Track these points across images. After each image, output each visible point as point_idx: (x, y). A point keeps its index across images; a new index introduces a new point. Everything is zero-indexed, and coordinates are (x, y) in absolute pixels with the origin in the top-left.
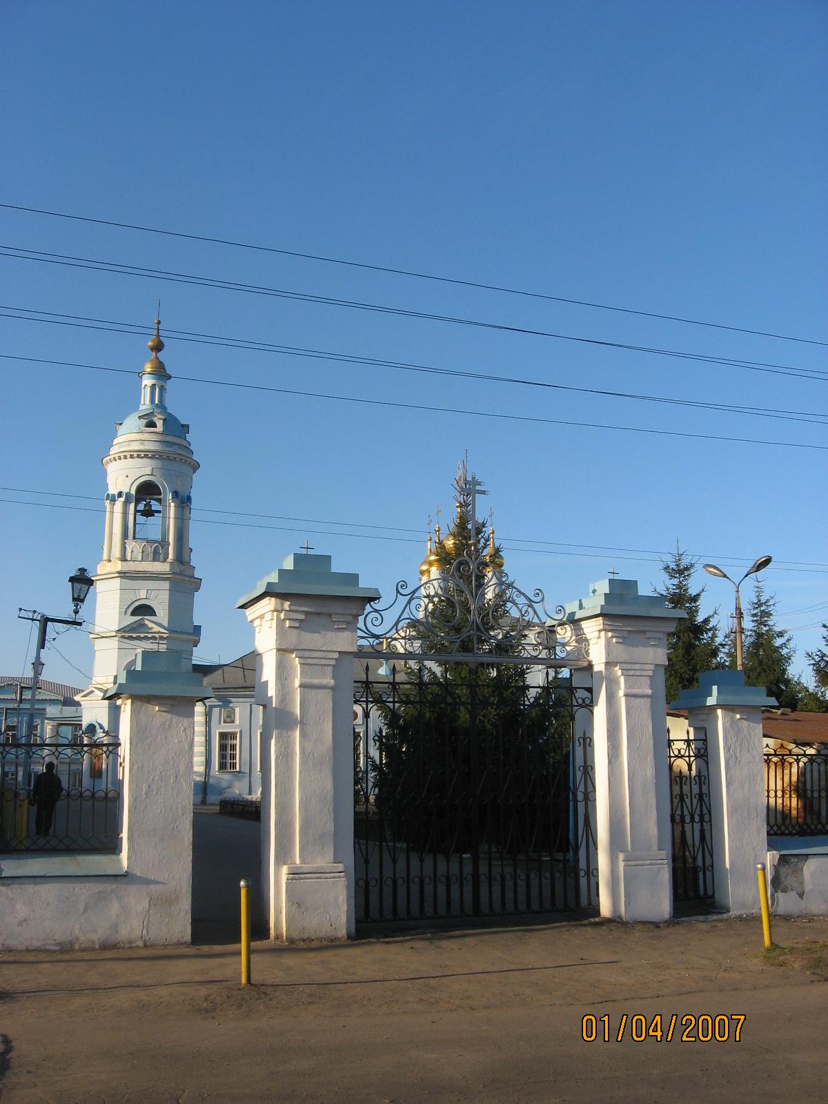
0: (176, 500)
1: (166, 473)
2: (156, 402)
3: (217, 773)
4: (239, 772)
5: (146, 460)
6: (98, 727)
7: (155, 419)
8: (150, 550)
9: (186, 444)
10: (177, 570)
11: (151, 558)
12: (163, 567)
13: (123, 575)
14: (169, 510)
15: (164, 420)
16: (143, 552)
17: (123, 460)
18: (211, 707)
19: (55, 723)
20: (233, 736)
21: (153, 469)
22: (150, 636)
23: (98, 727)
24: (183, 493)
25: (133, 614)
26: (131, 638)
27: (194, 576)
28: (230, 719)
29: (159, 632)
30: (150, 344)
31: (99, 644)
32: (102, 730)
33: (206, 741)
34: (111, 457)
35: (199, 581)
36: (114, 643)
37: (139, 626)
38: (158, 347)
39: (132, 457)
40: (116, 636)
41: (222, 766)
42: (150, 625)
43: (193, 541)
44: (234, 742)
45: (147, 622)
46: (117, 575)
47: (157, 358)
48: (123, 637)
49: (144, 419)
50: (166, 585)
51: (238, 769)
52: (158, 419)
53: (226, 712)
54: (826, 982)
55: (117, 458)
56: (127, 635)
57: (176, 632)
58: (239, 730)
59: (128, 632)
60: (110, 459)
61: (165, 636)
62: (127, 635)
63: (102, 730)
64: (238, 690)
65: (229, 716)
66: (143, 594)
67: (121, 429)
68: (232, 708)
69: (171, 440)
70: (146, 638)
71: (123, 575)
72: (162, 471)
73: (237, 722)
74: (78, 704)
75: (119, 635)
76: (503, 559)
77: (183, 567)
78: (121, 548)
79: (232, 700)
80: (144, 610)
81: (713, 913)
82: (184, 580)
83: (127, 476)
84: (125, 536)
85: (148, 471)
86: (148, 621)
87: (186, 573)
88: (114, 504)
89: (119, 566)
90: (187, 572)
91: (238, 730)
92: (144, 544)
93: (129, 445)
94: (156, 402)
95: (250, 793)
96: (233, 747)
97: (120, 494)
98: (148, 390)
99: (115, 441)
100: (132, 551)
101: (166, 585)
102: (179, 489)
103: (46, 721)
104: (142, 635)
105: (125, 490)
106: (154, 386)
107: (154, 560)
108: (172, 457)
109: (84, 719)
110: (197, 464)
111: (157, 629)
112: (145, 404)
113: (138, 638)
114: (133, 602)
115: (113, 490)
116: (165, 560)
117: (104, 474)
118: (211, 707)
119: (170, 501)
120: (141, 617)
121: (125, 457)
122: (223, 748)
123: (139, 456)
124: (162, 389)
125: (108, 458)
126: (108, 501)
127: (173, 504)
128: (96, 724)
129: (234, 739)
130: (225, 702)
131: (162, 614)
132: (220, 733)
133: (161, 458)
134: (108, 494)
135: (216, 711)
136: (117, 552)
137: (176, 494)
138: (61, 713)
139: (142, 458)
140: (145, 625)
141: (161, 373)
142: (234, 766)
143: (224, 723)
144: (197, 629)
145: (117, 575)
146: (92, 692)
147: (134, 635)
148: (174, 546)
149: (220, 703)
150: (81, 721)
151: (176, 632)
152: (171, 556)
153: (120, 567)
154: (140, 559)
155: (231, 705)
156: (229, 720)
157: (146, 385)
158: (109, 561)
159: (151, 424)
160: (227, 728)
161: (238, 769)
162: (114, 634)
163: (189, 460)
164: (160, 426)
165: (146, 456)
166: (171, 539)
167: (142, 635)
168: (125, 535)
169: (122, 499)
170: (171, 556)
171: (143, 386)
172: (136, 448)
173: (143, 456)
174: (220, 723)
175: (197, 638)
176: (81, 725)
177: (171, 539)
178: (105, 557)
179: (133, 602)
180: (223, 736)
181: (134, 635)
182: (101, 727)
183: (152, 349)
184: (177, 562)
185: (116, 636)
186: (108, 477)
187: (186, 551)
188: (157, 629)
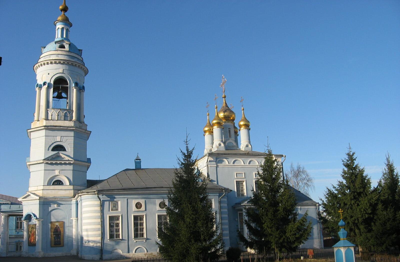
0: (77, 87)
1: (71, 73)
2: (65, 37)
3: (108, 241)
4: (122, 240)
5: (59, 65)
6: (33, 216)
7: (64, 44)
8: (62, 114)
9: (81, 59)
10: (78, 126)
11: (63, 118)
12: (71, 124)
13: (47, 128)
14: (73, 92)
15: (70, 45)
16: (58, 115)
17: (46, 65)
18: (104, 201)
19: (7, 214)
20: (117, 218)
21: (63, 70)
22: (63, 162)
23: (33, 216)
24: (81, 84)
25: (53, 150)
26: (52, 164)
27: (87, 130)
28: (115, 208)
29: (69, 160)
30: (61, 7)
31: (32, 168)
32: (35, 218)
33: (101, 221)
34: (39, 64)
35: (89, 133)
36: (42, 166)
37: (57, 157)
38: (65, 9)
39: (51, 63)
40: (43, 163)
41: (111, 236)
42: (63, 156)
43: (86, 111)
44: (117, 222)
45: (61, 155)
46: (43, 128)
47: (64, 15)
48: (47, 163)
49: (59, 43)
50: (72, 134)
51: (121, 238)
52: (66, 44)
53: (112, 204)
54: (346, 261)
55: (43, 64)
56: (49, 162)
57: (78, 160)
58: (145, 214)
59: (50, 160)
60: (39, 65)
61: (72, 162)
62: (49, 162)
63: (35, 218)
64: (120, 190)
65: (114, 207)
66: (58, 139)
67: (44, 50)
68: (116, 201)
69: (73, 55)
70: (61, 164)
71: (47, 128)
72: (69, 71)
73: (120, 209)
74: (20, 204)
75: (45, 162)
76: (250, 123)
77: (81, 125)
78: (46, 112)
79: (116, 197)
80: (59, 148)
81: (98, 247)
82: (82, 132)
83: (49, 74)
84: (48, 106)
85: (61, 71)
86: (62, 154)
87: (82, 128)
88: (41, 90)
89: (44, 123)
90: (83, 128)
91: (120, 215)
92: (59, 111)
93: (50, 57)
94: (65, 37)
95: (129, 252)
96: (117, 225)
97: (45, 84)
98: (60, 31)
99: (40, 61)
100: (52, 115)
101: (72, 134)
102: (78, 82)
103: (1, 213)
104: (58, 162)
105: (48, 81)
106: (63, 29)
107: (65, 120)
108: (74, 64)
109: (24, 211)
110: (87, 72)
111: (67, 158)
112: (58, 37)
113: (56, 164)
114: (53, 144)
115: (40, 82)
116: (71, 120)
117: (34, 75)
118: (104, 201)
119: (74, 88)
120: (57, 152)
121: (48, 64)
122: (136, 224)
123: (55, 63)
124: (67, 30)
125: (37, 65)
126: (38, 88)
127: (75, 90)
128: (32, 214)
129: (118, 220)
130: (112, 198)
131: (70, 150)
132: (110, 217)
133: (68, 64)
134: (38, 84)
135: (107, 204)
136: (43, 115)
137: (76, 84)
138: (10, 209)
139: (57, 64)
140: (59, 156)
141: (66, 21)
142: (118, 236)
143: (112, 210)
144: (89, 161)
145: (43, 128)
146: (29, 195)
147: (54, 162)
148: (76, 112)
149: (109, 199)
150: (22, 213)
151: (78, 160)
152: (74, 118)
153: (45, 124)
154: (57, 119)
155: (115, 200)
156: (114, 208)
157: (59, 28)
158: (38, 121)
159: (62, 47)
160: (114, 214)
161: (121, 238)
162: (42, 161)
163: (83, 67)
164: (67, 47)
165: (60, 63)
166: (74, 109)
167: (58, 162)
168: (48, 103)
169: (46, 86)
170: (74, 118)
171: (57, 29)
172: (54, 59)
173: (58, 62)
174: (109, 211)
175: (89, 164)
176: (22, 215)
177: (74, 109)
178: (36, 118)
179: (53, 144)
180: (111, 218)
181: (54, 162)
182: (35, 216)
183: (62, 10)
184: (77, 121)
185: (43, 163)
186: (37, 76)
187: (82, 117)
188: (67, 158)
